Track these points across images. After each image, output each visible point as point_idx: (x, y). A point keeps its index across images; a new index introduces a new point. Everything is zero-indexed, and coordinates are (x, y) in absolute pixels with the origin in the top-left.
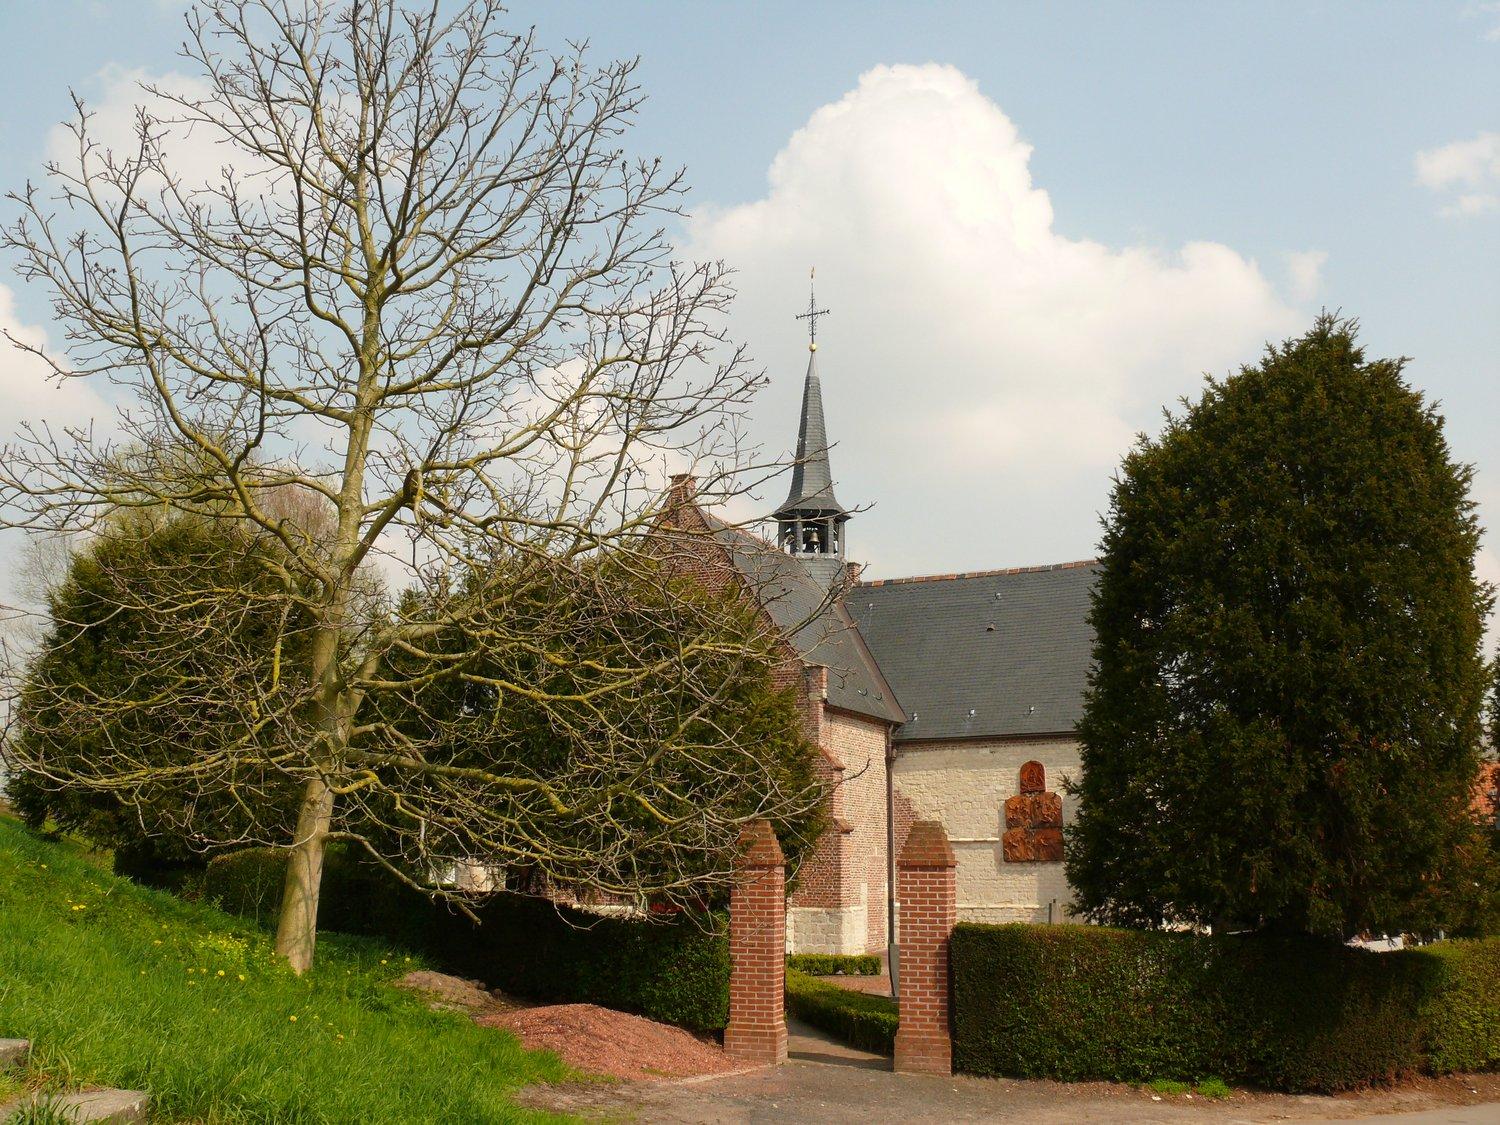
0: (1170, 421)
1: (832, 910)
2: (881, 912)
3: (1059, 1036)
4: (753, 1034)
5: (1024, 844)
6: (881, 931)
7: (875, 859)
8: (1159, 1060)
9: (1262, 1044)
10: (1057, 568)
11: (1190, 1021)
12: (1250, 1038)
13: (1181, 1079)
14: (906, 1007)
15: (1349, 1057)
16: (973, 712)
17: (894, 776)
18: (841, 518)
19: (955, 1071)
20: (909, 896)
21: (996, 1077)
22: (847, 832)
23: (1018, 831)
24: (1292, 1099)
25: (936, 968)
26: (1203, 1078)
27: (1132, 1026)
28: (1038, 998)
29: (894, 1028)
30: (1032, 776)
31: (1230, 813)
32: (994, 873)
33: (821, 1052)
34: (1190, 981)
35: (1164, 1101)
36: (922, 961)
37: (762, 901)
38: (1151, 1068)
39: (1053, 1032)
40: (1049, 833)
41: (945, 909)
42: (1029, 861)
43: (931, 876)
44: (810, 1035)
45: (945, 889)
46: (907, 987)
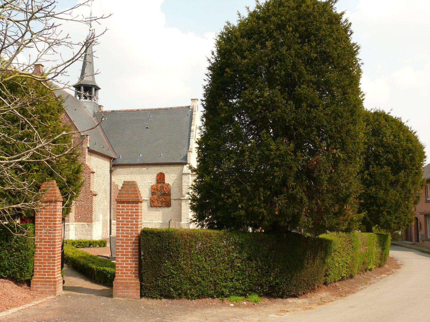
0: (240, 17)
1: (89, 223)
2: (107, 224)
3: (190, 279)
4: (45, 281)
5: (157, 201)
6: (107, 231)
7: (105, 206)
8: (233, 288)
9: (275, 279)
10: (171, 108)
11: (246, 270)
12: (270, 276)
13: (241, 295)
14: (119, 267)
15: (305, 282)
16: (141, 155)
17: (112, 176)
18: (97, 88)
19: (141, 296)
20: (121, 215)
21: (160, 299)
22: (95, 195)
23: (155, 196)
24: (285, 301)
25: (133, 249)
26: (250, 294)
27: (221, 273)
28: (180, 262)
29: (113, 275)
30: (161, 178)
31: (269, 179)
32: (147, 211)
33: (80, 286)
34: (247, 253)
35: (235, 306)
36: (126, 246)
37: (51, 218)
38: (229, 291)
39: (187, 278)
40: (166, 197)
41: (137, 222)
42: (159, 207)
43: (132, 206)
44: (75, 276)
45: (138, 212)
46: (119, 258)
